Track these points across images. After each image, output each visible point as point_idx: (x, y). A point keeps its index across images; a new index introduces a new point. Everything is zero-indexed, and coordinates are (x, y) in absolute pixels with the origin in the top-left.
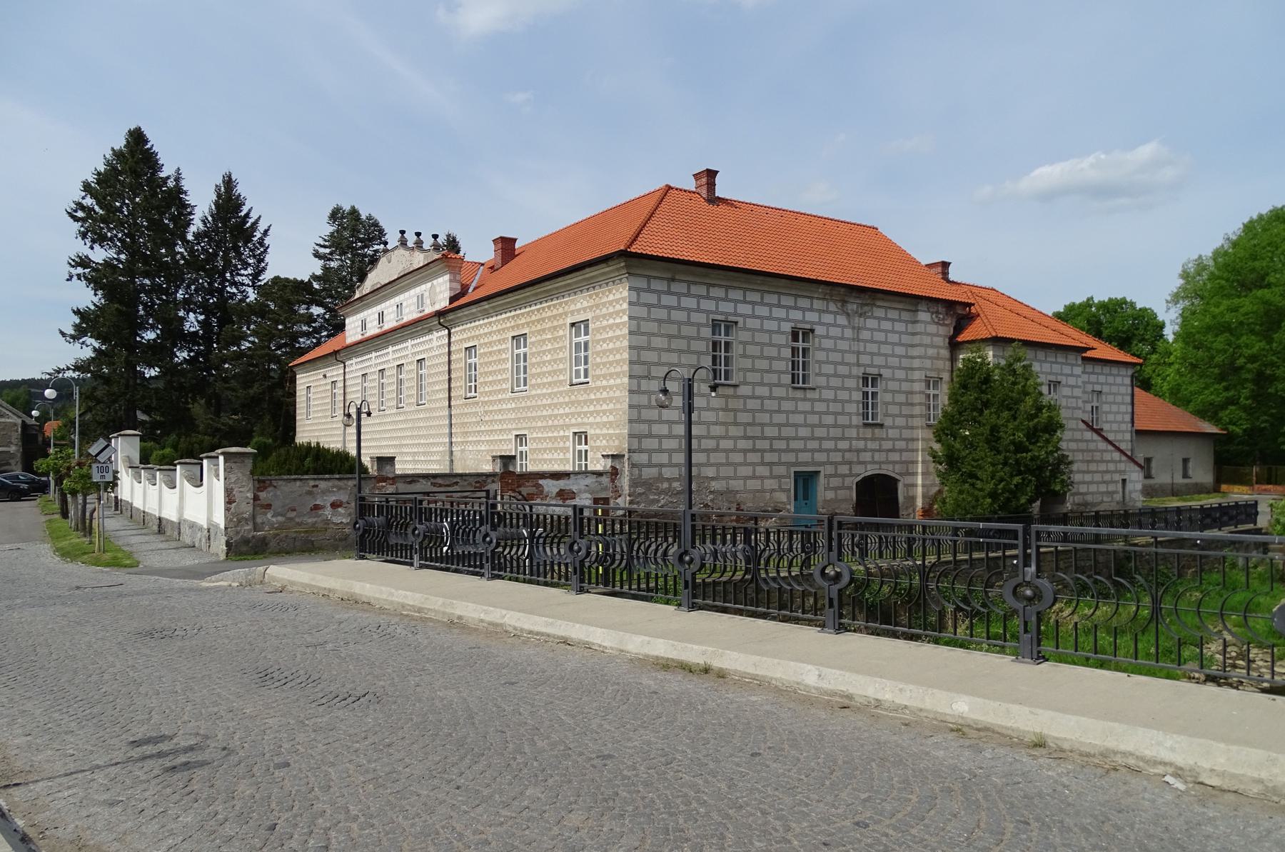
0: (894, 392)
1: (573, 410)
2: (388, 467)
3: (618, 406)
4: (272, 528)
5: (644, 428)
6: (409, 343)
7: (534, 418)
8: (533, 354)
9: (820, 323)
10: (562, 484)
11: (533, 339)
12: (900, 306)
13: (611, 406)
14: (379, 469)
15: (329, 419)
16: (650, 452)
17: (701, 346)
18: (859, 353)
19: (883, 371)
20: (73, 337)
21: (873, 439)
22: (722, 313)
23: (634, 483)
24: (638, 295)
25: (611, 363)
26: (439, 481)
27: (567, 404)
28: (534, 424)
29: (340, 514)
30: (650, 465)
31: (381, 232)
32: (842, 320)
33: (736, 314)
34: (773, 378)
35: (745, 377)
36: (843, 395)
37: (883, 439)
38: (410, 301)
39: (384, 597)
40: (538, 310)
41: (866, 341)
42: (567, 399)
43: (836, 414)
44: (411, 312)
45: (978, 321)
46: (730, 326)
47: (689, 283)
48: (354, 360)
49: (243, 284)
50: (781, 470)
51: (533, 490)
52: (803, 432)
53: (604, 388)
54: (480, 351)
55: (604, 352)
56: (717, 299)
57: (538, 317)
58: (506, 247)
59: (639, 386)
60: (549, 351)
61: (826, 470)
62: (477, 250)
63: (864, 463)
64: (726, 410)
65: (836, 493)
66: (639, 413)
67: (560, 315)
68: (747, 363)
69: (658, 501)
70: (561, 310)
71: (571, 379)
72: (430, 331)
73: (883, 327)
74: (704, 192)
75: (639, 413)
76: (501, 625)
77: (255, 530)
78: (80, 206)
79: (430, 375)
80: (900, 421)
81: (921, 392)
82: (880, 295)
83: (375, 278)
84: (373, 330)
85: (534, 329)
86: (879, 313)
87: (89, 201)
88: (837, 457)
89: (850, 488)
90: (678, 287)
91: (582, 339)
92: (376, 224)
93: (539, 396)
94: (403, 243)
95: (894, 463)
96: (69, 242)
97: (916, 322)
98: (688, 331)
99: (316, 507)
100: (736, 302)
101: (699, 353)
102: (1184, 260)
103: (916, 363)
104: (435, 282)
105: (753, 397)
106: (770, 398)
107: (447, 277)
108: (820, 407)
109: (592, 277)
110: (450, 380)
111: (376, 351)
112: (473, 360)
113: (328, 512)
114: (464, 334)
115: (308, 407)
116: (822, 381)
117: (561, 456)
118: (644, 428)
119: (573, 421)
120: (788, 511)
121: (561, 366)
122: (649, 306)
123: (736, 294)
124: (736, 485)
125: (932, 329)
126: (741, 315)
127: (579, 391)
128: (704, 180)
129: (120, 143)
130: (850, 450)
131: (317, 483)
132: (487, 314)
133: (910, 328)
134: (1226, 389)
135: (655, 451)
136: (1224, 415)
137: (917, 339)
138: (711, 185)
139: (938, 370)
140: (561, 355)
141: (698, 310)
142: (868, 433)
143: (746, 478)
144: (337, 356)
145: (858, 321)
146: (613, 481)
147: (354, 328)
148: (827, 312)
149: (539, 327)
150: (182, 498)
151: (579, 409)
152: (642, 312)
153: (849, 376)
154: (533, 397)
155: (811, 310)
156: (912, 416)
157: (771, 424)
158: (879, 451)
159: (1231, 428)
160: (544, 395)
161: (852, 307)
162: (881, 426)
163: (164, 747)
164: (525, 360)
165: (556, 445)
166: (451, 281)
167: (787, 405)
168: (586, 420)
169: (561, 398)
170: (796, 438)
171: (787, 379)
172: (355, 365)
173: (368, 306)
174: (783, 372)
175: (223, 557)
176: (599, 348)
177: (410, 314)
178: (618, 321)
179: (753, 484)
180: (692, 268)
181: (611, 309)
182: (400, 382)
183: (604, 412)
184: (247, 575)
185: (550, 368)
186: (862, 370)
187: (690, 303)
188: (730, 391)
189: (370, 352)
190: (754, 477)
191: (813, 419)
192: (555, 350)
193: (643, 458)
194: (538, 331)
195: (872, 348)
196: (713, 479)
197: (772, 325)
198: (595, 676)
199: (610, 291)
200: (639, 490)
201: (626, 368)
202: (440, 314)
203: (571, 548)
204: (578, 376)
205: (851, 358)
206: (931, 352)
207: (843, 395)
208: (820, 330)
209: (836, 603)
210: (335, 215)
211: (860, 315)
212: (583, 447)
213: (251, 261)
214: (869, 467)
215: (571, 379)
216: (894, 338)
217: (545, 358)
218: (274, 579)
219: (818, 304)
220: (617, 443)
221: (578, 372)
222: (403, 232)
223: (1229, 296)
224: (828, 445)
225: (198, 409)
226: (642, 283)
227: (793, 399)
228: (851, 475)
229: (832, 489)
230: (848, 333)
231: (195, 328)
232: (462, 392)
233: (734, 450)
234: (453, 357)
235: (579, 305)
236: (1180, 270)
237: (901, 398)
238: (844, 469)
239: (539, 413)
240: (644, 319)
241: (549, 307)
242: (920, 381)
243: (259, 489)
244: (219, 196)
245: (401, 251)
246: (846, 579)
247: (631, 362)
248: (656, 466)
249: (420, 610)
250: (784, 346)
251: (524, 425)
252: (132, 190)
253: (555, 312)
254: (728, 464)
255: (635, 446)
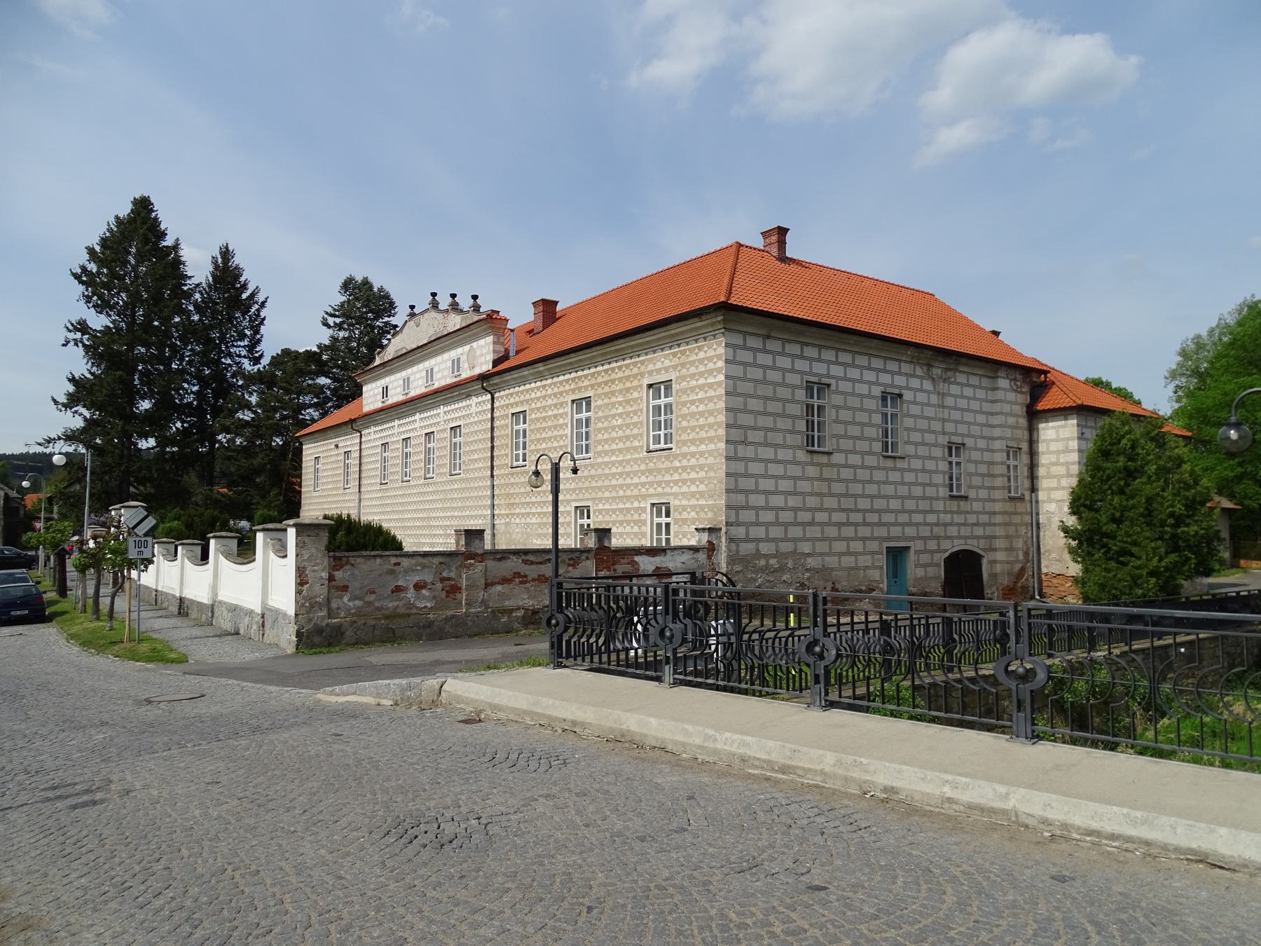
0: (976, 462)
1: (651, 478)
2: (477, 542)
3: (712, 474)
4: (349, 613)
5: (741, 498)
6: (442, 409)
7: (600, 488)
8: (532, 431)
9: (908, 388)
10: (658, 561)
11: (600, 402)
12: (981, 372)
13: (702, 474)
14: (467, 544)
15: (341, 492)
16: (748, 525)
17: (796, 410)
18: (944, 420)
19: (966, 440)
20: (64, 405)
21: (959, 512)
22: (816, 375)
23: (732, 560)
24: (735, 352)
25: (702, 427)
26: (531, 558)
27: (643, 473)
28: (600, 495)
29: (425, 598)
30: (748, 540)
31: (392, 305)
32: (928, 385)
33: (828, 376)
34: (863, 446)
35: (838, 444)
36: (930, 465)
37: (968, 513)
38: (418, 376)
39: (698, 741)
40: (606, 371)
41: (950, 408)
42: (643, 467)
43: (924, 485)
44: (444, 377)
45: (1054, 389)
46: (823, 387)
47: (785, 341)
48: (373, 429)
49: (239, 356)
50: (874, 546)
51: (628, 568)
52: (895, 504)
53: (693, 455)
54: (437, 436)
55: (692, 415)
56: (811, 359)
57: (606, 378)
58: (547, 309)
59: (736, 452)
60: (620, 415)
61: (917, 545)
62: (520, 315)
63: (951, 538)
64: (821, 479)
65: (925, 570)
66: (736, 481)
67: (635, 376)
68: (839, 429)
69: (755, 580)
70: (635, 371)
71: (648, 446)
72: (468, 396)
73: (966, 392)
74: (774, 250)
75: (736, 481)
76: (1004, 812)
77: (330, 616)
78: (84, 268)
79: (467, 443)
80: (983, 494)
81: (1002, 463)
82: (964, 360)
83: (395, 346)
84: (396, 397)
85: (600, 391)
86: (961, 378)
87: (93, 267)
88: (925, 531)
89: (938, 565)
90: (774, 345)
91: (521, 427)
92: (387, 297)
93: (606, 464)
94: (435, 305)
95: (978, 537)
96: (73, 304)
97: (994, 389)
98: (783, 393)
99: (398, 589)
100: (829, 362)
101: (793, 417)
102: (1183, 338)
103: (997, 432)
104: (474, 345)
105: (846, 466)
106: (863, 467)
107: (490, 339)
108: (909, 477)
109: (676, 334)
110: (493, 447)
111: (399, 418)
112: (458, 440)
113: (411, 594)
114: (509, 399)
115: (316, 478)
116: (910, 450)
117: (636, 529)
118: (741, 498)
119: (651, 491)
120: (881, 590)
121: (636, 431)
122: (745, 364)
123: (829, 355)
124: (831, 561)
125: (1011, 396)
126: (833, 377)
127: (659, 458)
128: (774, 238)
129: (125, 210)
130: (937, 524)
131: (399, 560)
132: (541, 376)
133: (991, 396)
134: (1240, 464)
135: (752, 524)
136: (1238, 489)
137: (997, 407)
138: (782, 244)
139: (1018, 440)
140: (635, 419)
141: (793, 371)
142: (954, 505)
143: (841, 554)
144: (354, 425)
145: (942, 387)
146: (709, 557)
147: (372, 396)
148: (914, 376)
149: (607, 389)
150: (216, 576)
151: (659, 478)
152: (738, 371)
153: (935, 445)
154: (599, 465)
155: (900, 373)
156: (993, 488)
157: (864, 496)
158: (964, 524)
159: (1246, 502)
160: (613, 463)
161: (937, 372)
162: (966, 498)
163: (70, 790)
164: (525, 436)
165: (629, 517)
166: (494, 343)
167: (879, 475)
168: (668, 490)
169: (656, 464)
170: (888, 511)
171: (877, 447)
172: (373, 435)
173: (391, 373)
174: (874, 440)
175: (291, 649)
176: (685, 411)
177: (443, 378)
178: (711, 380)
179: (848, 561)
180: (790, 325)
181: (702, 368)
182: (428, 451)
183: (693, 481)
184: (403, 690)
185: (620, 433)
186: (947, 438)
187: (785, 362)
188: (824, 459)
189: (393, 420)
190: (848, 553)
191: (903, 490)
192: (628, 414)
193: (740, 532)
194: (606, 394)
195: (956, 415)
196: (809, 555)
197: (862, 389)
198: (782, 801)
199: (700, 348)
200: (738, 568)
201: (722, 432)
202: (483, 377)
203: (662, 633)
204: (517, 460)
205: (937, 426)
206: (1011, 420)
207: (930, 465)
208: (908, 395)
209: (822, 679)
210: (348, 285)
211: (945, 381)
212: (664, 520)
213: (248, 333)
214: (956, 542)
215: (648, 446)
216: (975, 405)
217: (614, 423)
218: (459, 699)
219: (906, 368)
220: (710, 515)
221: (517, 455)
222: (434, 295)
223: (1238, 374)
224: (918, 518)
225: (191, 478)
226: (738, 340)
227: (884, 468)
228: (939, 551)
229: (922, 566)
230: (934, 399)
231: (194, 396)
232: (508, 461)
233: (829, 524)
234: (497, 423)
235: (660, 363)
236: (1178, 348)
237: (983, 469)
238: (932, 545)
239: (607, 483)
240: (739, 379)
241: (620, 368)
242: (1001, 451)
243: (335, 568)
244: (216, 267)
245: (433, 314)
246: (1041, 676)
247: (728, 426)
248: (753, 540)
249: (784, 769)
250: (875, 412)
251: (587, 496)
252: (133, 255)
253: (627, 373)
254: (823, 539)
255: (733, 519)
